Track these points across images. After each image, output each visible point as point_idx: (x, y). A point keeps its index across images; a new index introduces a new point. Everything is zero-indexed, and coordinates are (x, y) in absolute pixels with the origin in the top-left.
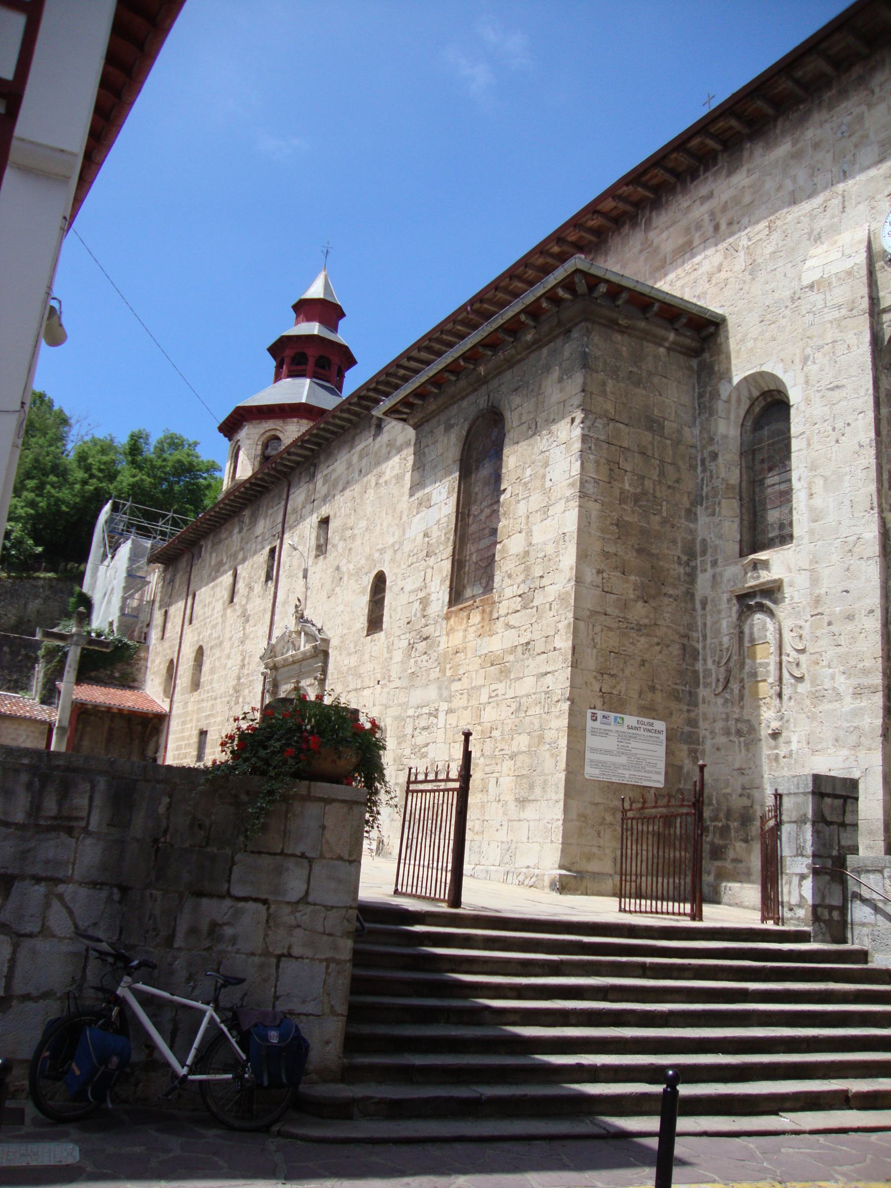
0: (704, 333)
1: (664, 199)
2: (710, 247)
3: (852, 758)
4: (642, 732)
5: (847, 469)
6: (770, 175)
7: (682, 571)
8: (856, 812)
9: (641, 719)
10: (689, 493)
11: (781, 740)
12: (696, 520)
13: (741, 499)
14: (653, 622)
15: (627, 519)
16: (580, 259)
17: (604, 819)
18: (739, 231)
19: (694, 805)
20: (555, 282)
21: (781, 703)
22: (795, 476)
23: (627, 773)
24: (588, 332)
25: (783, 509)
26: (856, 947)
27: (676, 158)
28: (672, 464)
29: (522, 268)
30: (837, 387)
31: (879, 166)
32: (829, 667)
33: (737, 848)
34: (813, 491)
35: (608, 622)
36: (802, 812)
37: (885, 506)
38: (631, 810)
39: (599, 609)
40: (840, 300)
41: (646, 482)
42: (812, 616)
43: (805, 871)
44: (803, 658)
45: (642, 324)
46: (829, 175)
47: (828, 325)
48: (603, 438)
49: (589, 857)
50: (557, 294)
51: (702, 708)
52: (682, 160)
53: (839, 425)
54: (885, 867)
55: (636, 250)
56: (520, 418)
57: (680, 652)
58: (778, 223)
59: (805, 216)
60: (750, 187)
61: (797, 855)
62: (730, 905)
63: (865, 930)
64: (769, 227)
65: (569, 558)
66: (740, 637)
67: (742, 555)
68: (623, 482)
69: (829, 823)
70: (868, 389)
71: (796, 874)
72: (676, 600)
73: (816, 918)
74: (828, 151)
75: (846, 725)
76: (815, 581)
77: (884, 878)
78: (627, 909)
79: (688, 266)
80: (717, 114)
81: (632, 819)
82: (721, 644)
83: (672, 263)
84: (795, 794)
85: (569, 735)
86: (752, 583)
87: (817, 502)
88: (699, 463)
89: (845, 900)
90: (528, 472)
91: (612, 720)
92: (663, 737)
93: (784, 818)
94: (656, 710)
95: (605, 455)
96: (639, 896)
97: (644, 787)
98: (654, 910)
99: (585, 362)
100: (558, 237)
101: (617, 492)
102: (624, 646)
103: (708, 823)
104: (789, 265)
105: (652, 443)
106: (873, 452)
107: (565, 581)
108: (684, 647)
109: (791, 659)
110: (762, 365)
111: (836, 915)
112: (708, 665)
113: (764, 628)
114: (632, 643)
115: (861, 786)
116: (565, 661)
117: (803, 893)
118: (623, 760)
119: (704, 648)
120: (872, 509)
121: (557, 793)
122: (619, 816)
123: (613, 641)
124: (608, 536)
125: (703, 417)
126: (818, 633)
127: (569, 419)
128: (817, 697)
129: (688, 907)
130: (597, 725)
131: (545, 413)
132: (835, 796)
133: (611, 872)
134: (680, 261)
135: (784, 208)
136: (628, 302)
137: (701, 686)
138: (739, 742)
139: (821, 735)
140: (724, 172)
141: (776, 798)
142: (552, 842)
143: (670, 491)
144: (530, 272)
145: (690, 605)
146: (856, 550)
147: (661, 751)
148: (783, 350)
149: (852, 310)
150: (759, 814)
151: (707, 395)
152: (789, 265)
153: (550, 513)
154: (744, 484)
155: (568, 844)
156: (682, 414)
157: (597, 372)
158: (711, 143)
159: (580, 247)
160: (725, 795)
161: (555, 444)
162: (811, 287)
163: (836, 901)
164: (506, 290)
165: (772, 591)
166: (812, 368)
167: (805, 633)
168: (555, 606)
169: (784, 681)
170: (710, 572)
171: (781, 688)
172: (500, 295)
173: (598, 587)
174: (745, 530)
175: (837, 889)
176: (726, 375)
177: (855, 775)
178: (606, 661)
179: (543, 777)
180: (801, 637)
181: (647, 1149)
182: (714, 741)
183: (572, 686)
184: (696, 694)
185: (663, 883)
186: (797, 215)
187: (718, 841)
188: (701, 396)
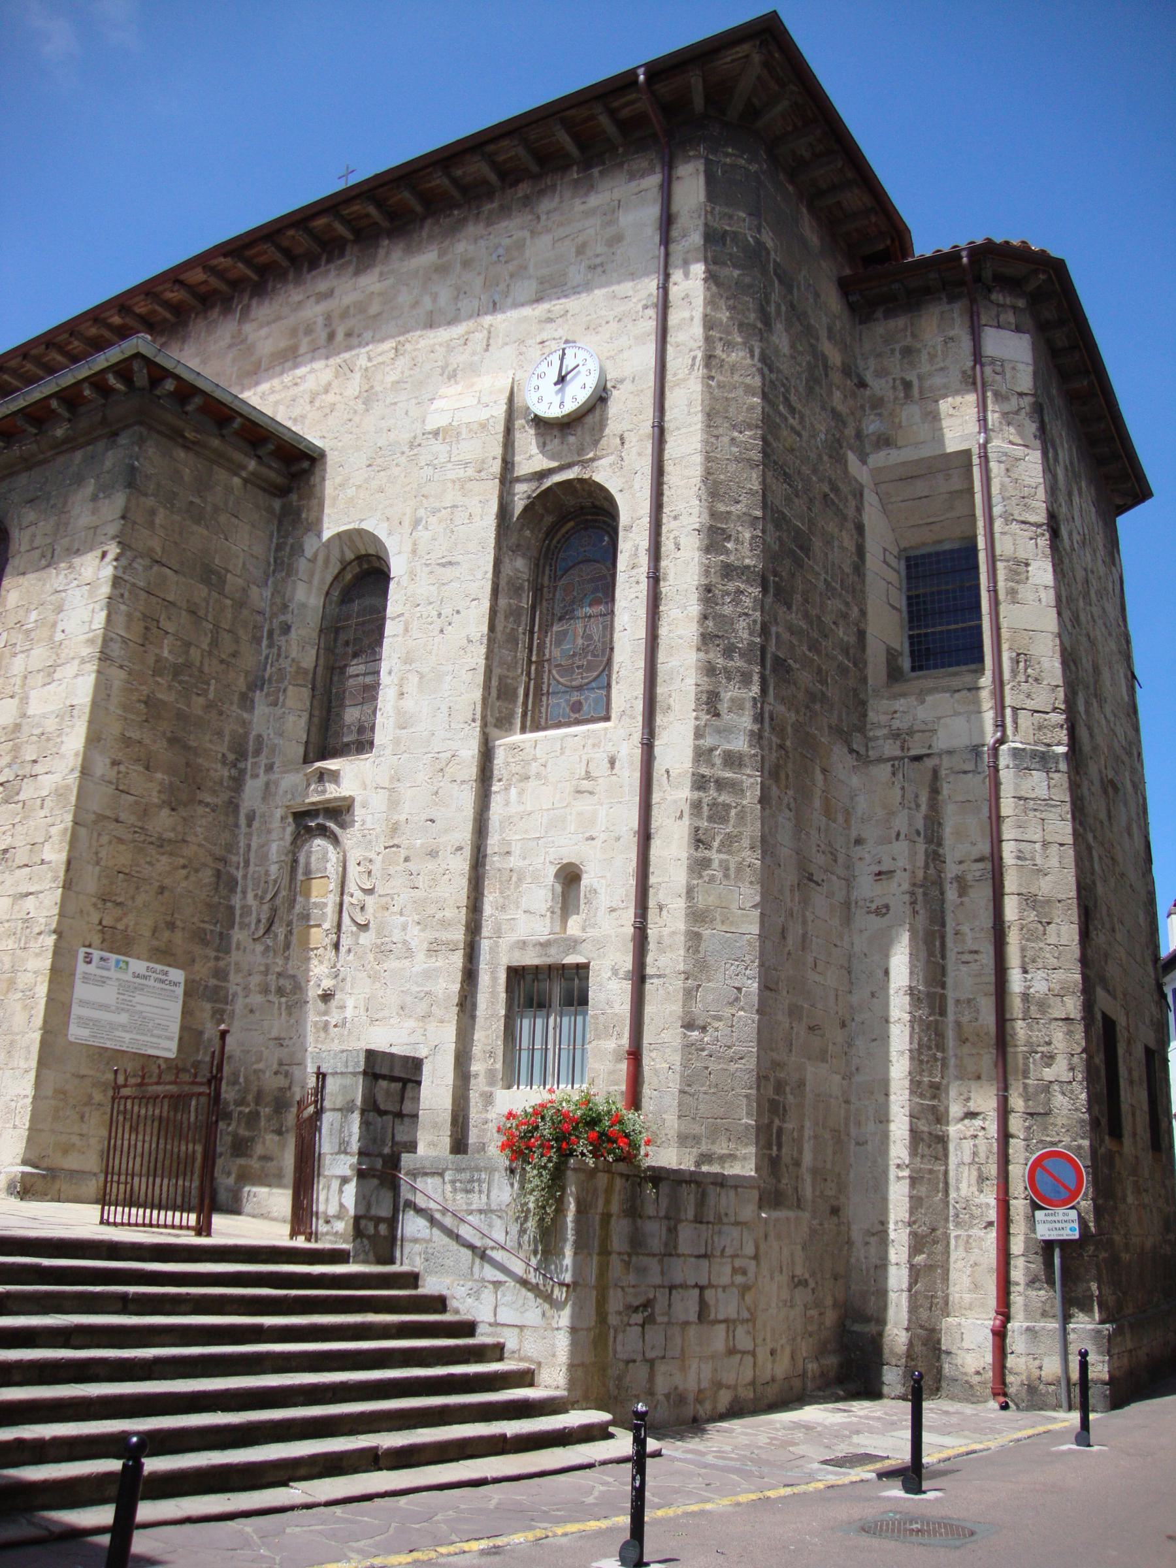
0: (295, 469)
1: (270, 285)
2: (320, 359)
3: (421, 1031)
4: (151, 983)
5: (450, 668)
6: (408, 285)
7: (226, 774)
8: (417, 1099)
9: (152, 965)
10: (247, 673)
11: (334, 1003)
12: (253, 708)
13: (313, 689)
14: (180, 838)
15: (160, 696)
16: (144, 339)
17: (90, 1097)
18: (359, 345)
19: (209, 1082)
20: (106, 365)
21: (337, 956)
22: (384, 667)
23: (127, 1037)
24: (141, 441)
25: (365, 708)
26: (405, 1268)
27: (293, 237)
28: (229, 631)
29: (66, 336)
30: (450, 563)
31: (535, 306)
32: (401, 914)
33: (268, 1142)
34: (405, 690)
35: (120, 831)
36: (349, 1098)
37: (490, 719)
38: (125, 1086)
39: (108, 813)
40: (468, 457)
41: (192, 650)
42: (386, 848)
43: (348, 1172)
44: (370, 901)
45: (216, 443)
46: (476, 303)
47: (450, 485)
48: (141, 584)
49: (66, 1150)
50: (106, 380)
51: (235, 956)
52: (301, 241)
53: (447, 611)
54: (447, 1169)
55: (223, 344)
56: (32, 541)
57: (213, 879)
58: (408, 347)
59: (440, 345)
60: (380, 294)
61: (339, 1152)
62: (254, 1216)
63: (418, 1247)
64: (396, 349)
65: (75, 741)
66: (292, 867)
67: (307, 760)
68: (162, 647)
69: (382, 1113)
70: (486, 572)
71: (337, 1177)
72: (213, 811)
73: (358, 1231)
74: (479, 274)
75: (415, 989)
76: (394, 803)
77: (444, 1183)
78: (112, 1220)
79: (287, 378)
80: (353, 193)
81: (127, 1098)
82: (267, 873)
83: (266, 370)
84: (342, 1073)
85: (51, 982)
86: (315, 798)
87: (408, 704)
88: (265, 634)
89: (396, 1210)
90: (34, 616)
91: (112, 963)
92: (180, 991)
93: (327, 1104)
94: (173, 955)
95: (141, 608)
96: (131, 1202)
97: (150, 1056)
98: (147, 1221)
99: (132, 480)
100: (121, 303)
101: (151, 660)
102: (138, 865)
103: (232, 1107)
104: (414, 401)
105: (206, 600)
106: (483, 650)
107: (66, 771)
108: (218, 874)
109: (354, 901)
110: (362, 520)
111: (383, 1229)
112: (248, 900)
113: (325, 858)
114: (150, 863)
115: (426, 1069)
116: (55, 879)
117: (343, 1200)
118: (123, 1018)
119: (245, 876)
120: (474, 720)
121: (27, 1059)
122: (110, 1093)
123: (123, 857)
124: (133, 717)
125: (279, 576)
126: (392, 871)
127: (98, 553)
128: (383, 952)
129: (193, 1218)
130: (91, 969)
131: (67, 539)
132: (393, 1079)
133: (96, 1169)
134: (278, 369)
135: (417, 329)
136: (204, 409)
137: (236, 927)
138: (280, 1004)
139: (384, 1001)
140: (351, 269)
141: (318, 1078)
142: (15, 1127)
143: (224, 666)
144: (76, 343)
145: (231, 820)
146: (448, 770)
147: (176, 1009)
148: (391, 505)
149: (480, 471)
150: (298, 1098)
151: (288, 549)
152: (414, 401)
153: (57, 676)
154: (320, 670)
155: (37, 1130)
156: (251, 569)
157: (146, 495)
158: (341, 229)
159: (150, 325)
160: (255, 1071)
161: (76, 583)
162: (436, 433)
163: (384, 1211)
164: (37, 360)
165: (340, 811)
166: (422, 535)
167: (376, 868)
168: (49, 803)
169: (344, 928)
170: (263, 778)
171: (339, 937)
172: (29, 366)
173: (110, 782)
174: (314, 729)
175: (387, 1196)
176: (316, 526)
177: (421, 1053)
178: (112, 883)
179: (10, 1037)
180: (370, 873)
181: (97, 1546)
182: (248, 1000)
183: (62, 915)
184: (229, 937)
185: (163, 1186)
186: (432, 342)
187: (243, 1132)
188: (279, 548)
